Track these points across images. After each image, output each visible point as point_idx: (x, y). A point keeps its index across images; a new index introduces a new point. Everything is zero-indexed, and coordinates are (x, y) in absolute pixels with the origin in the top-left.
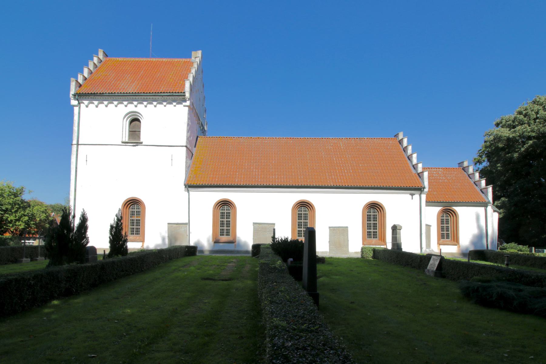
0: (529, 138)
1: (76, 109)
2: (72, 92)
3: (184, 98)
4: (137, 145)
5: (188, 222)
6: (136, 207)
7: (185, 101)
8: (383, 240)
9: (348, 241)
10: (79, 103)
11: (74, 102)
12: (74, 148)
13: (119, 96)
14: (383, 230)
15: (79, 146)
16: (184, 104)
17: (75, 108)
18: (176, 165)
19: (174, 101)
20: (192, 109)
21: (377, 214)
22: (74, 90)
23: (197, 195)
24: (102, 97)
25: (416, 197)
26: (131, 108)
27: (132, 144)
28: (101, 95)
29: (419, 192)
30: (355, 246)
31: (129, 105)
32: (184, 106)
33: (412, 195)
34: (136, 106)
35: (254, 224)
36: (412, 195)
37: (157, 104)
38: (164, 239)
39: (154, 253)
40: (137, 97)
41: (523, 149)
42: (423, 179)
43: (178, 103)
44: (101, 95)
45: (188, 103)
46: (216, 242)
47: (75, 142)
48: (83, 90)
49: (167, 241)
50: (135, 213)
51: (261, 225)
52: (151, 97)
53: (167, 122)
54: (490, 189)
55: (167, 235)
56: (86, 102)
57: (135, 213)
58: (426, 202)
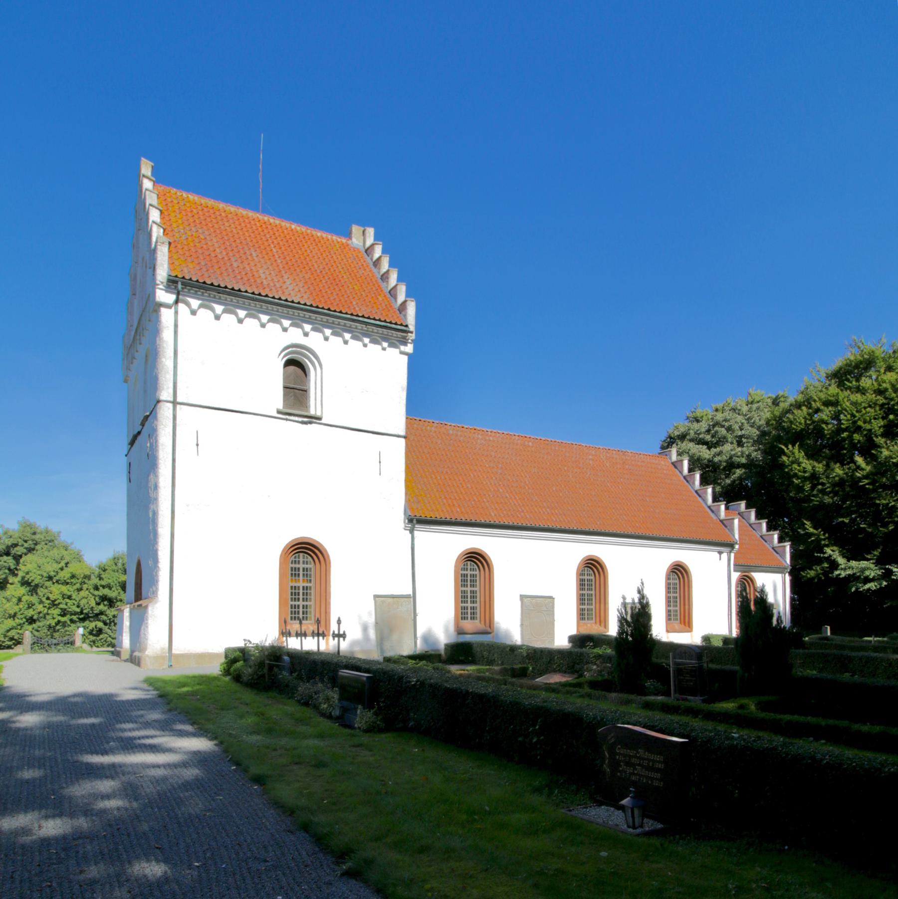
0: (739, 466)
1: (166, 316)
2: (162, 273)
3: (404, 338)
4: (311, 423)
5: (411, 593)
6: (301, 560)
7: (405, 343)
8: (604, 621)
9: (522, 625)
10: (177, 302)
11: (164, 296)
12: (165, 411)
13: (253, 299)
14: (687, 607)
15: (178, 407)
16: (402, 348)
17: (163, 310)
18: (383, 473)
19: (385, 339)
20: (414, 363)
21: (477, 572)
22: (166, 266)
23: (426, 537)
24: (235, 299)
25: (725, 556)
26: (295, 335)
27: (300, 419)
28: (235, 293)
29: (728, 549)
30: (563, 632)
31: (292, 330)
32: (402, 353)
33: (720, 553)
34: (306, 334)
35: (522, 597)
36: (720, 553)
37: (291, 325)
38: (365, 628)
39: (314, 663)
40: (313, 316)
41: (728, 481)
42: (732, 530)
43: (392, 345)
44: (235, 293)
45: (409, 348)
46: (460, 632)
47: (165, 394)
48: (190, 272)
49: (372, 634)
50: (301, 573)
51: (534, 601)
52: (342, 322)
53: (366, 378)
54: (787, 546)
55: (371, 620)
56: (195, 303)
57: (301, 573)
58: (735, 565)
